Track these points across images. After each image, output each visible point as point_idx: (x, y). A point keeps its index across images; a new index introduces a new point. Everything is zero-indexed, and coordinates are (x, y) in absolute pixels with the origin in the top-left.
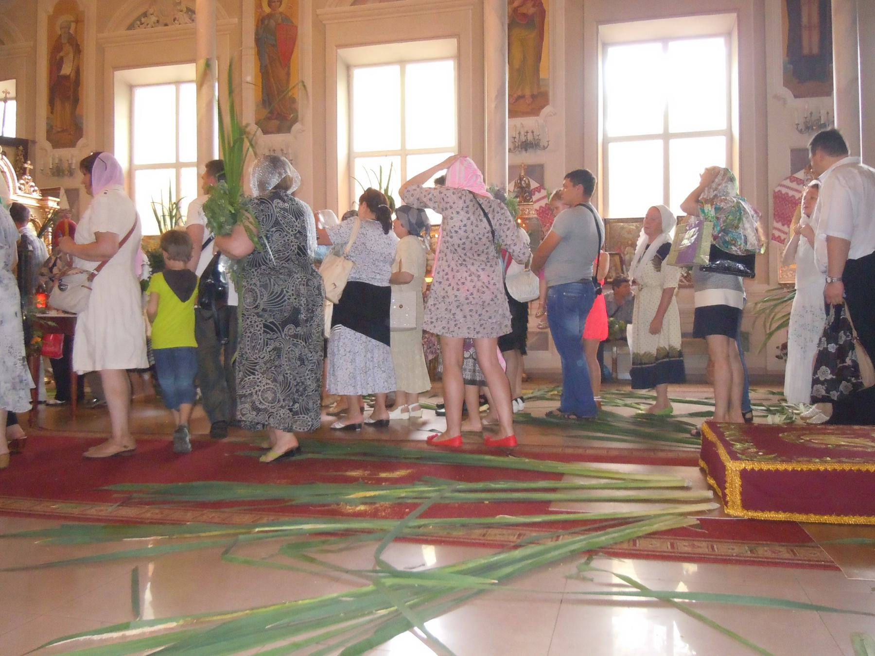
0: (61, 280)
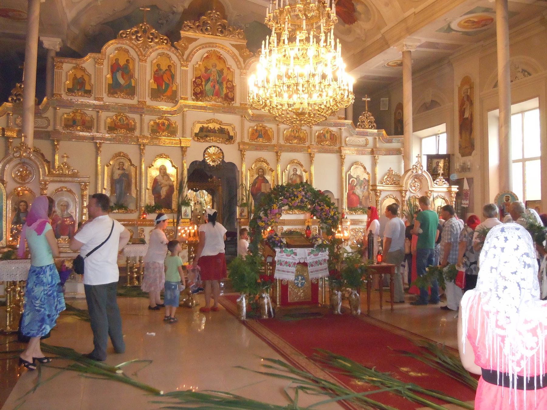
0: (36, 286)
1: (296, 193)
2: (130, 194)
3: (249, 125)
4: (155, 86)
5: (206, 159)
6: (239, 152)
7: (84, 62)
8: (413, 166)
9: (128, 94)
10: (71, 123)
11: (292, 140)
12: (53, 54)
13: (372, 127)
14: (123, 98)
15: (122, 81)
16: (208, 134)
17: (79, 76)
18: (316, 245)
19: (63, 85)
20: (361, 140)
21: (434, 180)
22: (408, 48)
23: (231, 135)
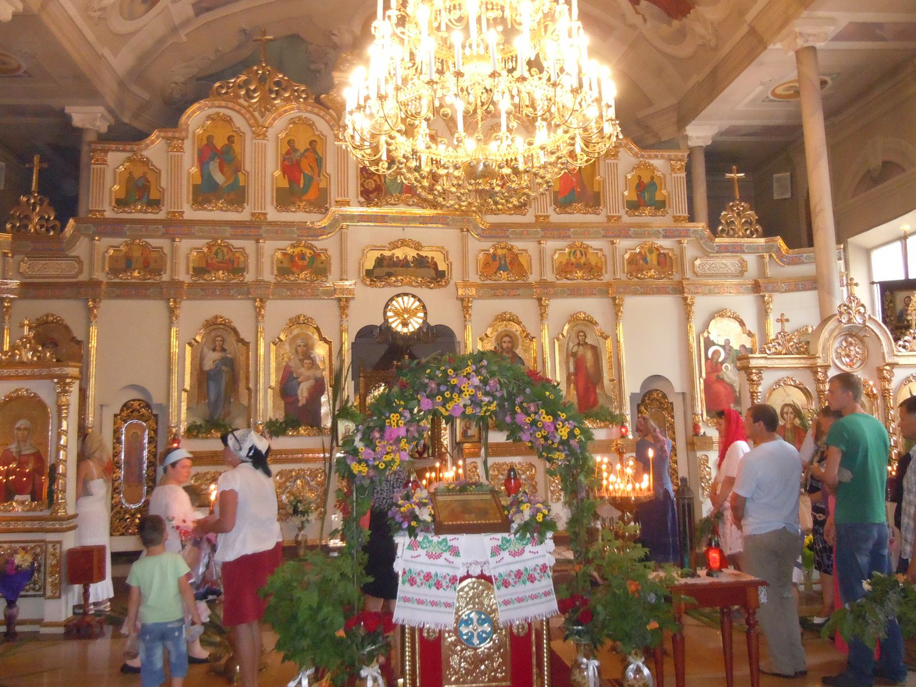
1: (454, 381)
2: (237, 399)
3: (478, 247)
4: (285, 184)
5: (390, 320)
6: (459, 302)
7: (147, 146)
8: (840, 307)
9: (231, 202)
10: (122, 265)
11: (571, 272)
12: (90, 137)
13: (752, 234)
14: (222, 210)
15: (219, 178)
16: (392, 270)
17: (137, 175)
18: (515, 526)
19: (107, 193)
20: (728, 263)
21: (896, 339)
22: (807, 41)
23: (440, 268)
